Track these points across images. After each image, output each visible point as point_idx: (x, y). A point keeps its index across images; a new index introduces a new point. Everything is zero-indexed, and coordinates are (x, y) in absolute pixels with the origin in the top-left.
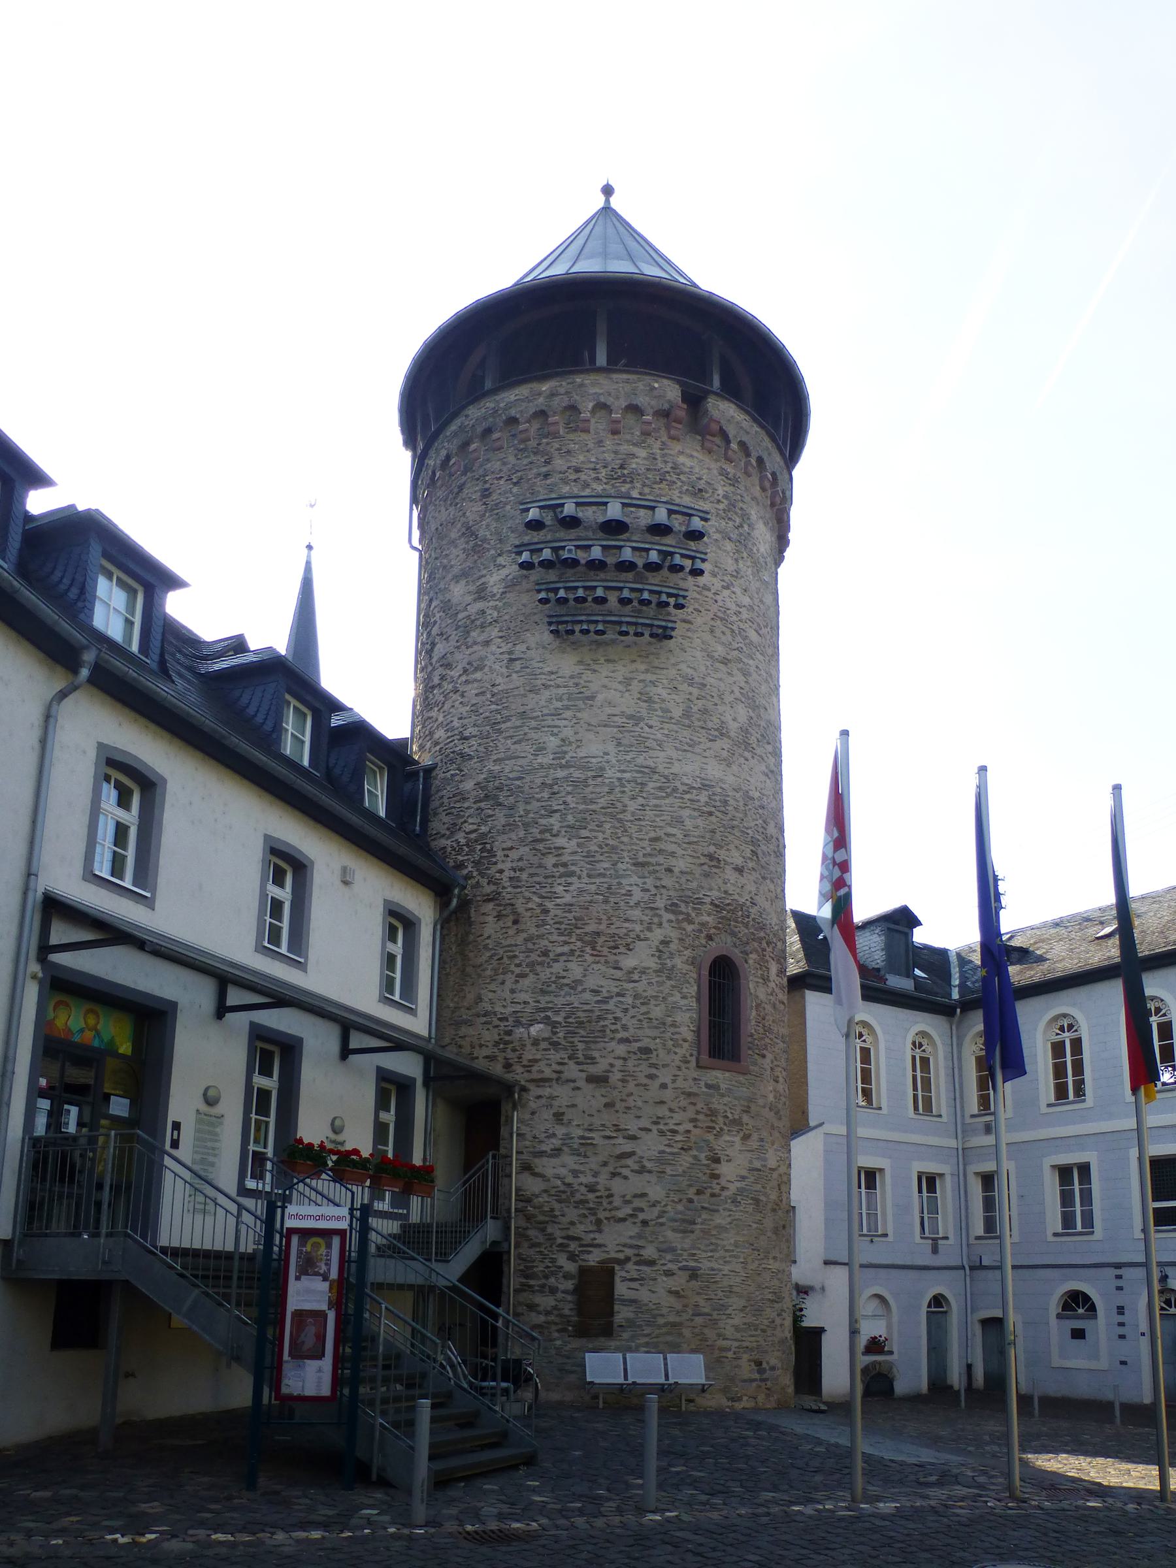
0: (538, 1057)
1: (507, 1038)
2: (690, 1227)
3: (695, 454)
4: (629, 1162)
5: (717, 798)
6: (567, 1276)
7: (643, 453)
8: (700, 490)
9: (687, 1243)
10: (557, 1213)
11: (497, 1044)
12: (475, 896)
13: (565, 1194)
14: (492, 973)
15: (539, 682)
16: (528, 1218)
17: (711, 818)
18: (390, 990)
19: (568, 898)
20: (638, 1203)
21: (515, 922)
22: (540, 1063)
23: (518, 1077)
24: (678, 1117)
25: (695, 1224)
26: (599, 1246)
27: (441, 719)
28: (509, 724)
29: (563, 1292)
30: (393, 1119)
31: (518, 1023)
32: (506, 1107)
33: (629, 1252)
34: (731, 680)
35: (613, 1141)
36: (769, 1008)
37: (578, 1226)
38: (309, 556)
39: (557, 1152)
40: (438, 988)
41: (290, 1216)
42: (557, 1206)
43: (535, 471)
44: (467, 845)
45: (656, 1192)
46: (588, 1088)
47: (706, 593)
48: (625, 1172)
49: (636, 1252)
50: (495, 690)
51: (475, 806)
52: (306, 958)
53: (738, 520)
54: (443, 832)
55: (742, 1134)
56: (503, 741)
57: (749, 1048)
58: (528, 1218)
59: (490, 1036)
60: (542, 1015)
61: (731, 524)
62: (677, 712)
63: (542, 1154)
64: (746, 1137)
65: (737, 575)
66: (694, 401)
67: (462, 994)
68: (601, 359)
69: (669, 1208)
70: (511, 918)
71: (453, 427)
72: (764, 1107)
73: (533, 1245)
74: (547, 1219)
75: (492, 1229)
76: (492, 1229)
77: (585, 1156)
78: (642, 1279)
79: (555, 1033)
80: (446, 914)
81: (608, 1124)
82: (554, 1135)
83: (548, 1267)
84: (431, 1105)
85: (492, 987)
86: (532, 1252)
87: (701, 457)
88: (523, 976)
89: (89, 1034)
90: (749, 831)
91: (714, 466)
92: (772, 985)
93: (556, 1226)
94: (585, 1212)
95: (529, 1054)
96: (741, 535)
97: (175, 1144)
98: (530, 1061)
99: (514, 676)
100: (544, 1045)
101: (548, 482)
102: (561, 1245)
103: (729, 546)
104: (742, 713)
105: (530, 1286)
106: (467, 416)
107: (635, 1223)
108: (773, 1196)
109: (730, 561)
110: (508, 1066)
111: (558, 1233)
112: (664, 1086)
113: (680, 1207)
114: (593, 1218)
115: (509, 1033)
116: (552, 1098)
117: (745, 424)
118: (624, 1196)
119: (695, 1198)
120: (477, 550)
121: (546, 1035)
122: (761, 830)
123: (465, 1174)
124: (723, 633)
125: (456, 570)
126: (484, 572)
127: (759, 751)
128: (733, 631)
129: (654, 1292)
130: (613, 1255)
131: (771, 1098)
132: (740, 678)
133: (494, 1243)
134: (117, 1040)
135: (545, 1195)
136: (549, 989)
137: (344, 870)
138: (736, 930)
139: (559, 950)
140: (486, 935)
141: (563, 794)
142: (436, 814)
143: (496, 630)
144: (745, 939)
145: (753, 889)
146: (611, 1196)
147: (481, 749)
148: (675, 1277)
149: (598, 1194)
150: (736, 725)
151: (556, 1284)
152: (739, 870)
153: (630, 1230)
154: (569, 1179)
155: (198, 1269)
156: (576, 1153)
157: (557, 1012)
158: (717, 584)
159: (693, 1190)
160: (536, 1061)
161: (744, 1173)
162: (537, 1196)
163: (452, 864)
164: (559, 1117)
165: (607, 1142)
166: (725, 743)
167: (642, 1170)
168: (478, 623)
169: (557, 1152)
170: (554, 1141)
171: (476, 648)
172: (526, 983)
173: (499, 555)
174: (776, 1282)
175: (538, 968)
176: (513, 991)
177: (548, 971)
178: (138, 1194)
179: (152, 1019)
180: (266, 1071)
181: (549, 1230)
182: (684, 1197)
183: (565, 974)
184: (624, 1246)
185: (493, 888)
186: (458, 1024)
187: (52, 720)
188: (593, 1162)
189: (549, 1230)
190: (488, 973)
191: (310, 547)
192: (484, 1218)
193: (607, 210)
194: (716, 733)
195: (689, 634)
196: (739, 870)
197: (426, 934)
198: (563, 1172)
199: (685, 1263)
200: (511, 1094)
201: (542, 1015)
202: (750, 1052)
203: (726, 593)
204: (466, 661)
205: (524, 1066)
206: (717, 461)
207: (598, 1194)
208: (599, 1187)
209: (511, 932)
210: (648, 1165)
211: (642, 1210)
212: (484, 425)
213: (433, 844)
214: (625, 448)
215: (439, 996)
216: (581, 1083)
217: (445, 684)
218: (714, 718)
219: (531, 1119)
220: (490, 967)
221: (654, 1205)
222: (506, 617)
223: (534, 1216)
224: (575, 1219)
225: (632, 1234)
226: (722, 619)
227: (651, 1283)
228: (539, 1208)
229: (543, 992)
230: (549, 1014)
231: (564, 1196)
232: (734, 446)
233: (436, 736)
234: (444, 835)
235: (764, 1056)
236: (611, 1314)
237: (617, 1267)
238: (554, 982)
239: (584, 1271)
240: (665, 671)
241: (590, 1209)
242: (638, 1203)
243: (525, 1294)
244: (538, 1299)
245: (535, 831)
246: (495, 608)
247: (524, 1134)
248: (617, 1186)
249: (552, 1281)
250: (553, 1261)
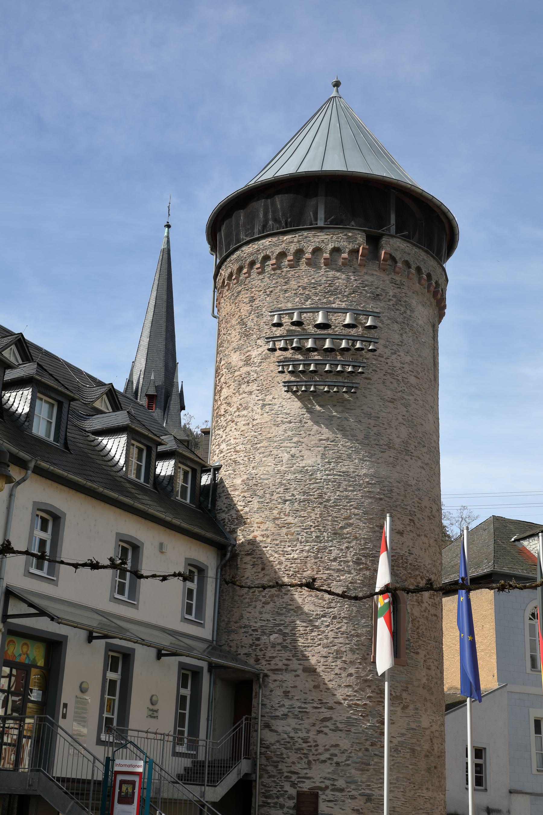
0: (274, 655)
1: (257, 642)
2: (366, 767)
3: (375, 273)
4: (328, 724)
5: (386, 489)
6: (290, 798)
8: (378, 295)
9: (365, 778)
10: (285, 756)
11: (251, 646)
12: (240, 551)
13: (289, 744)
14: (249, 601)
15: (279, 419)
16: (268, 758)
17: (381, 502)
18: (189, 612)
20: (333, 751)
21: (263, 569)
22: (276, 659)
23: (263, 668)
25: (369, 765)
26: (309, 778)
27: (224, 437)
28: (262, 445)
29: (287, 808)
30: (189, 693)
31: (264, 633)
32: (255, 687)
33: (328, 783)
34: (396, 411)
35: (318, 710)
36: (422, 621)
37: (297, 764)
39: (285, 716)
40: (219, 609)
41: (117, 765)
42: (284, 751)
43: (279, 288)
44: (237, 519)
45: (345, 744)
46: (303, 675)
47: (380, 359)
48: (326, 730)
49: (332, 782)
50: (255, 423)
51: (242, 495)
52: (138, 603)
53: (403, 309)
54: (224, 509)
55: (402, 705)
56: (258, 455)
57: (407, 649)
58: (268, 758)
59: (248, 641)
60: (278, 628)
61: (398, 312)
63: (276, 717)
64: (405, 708)
65: (401, 344)
66: (374, 241)
67: (232, 613)
69: (353, 754)
70: (261, 566)
71: (234, 256)
72: (418, 687)
73: (270, 777)
74: (279, 759)
75: (244, 766)
76: (244, 766)
77: (302, 719)
78: (336, 801)
79: (285, 640)
80: (224, 562)
81: (316, 699)
82: (284, 705)
83: (279, 791)
85: (249, 609)
86: (269, 781)
87: (378, 274)
89: (24, 657)
90: (408, 507)
91: (387, 278)
92: (425, 605)
93: (284, 764)
94: (302, 756)
95: (270, 653)
96: (405, 317)
97: (64, 716)
98: (270, 657)
99: (265, 415)
100: (279, 647)
101: (287, 295)
102: (287, 777)
103: (396, 327)
104: (404, 431)
105: (269, 803)
106: (242, 251)
107: (331, 764)
108: (426, 747)
109: (397, 336)
110: (257, 660)
111: (285, 769)
113: (360, 754)
114: (306, 760)
115: (258, 639)
116: (283, 681)
117: (407, 250)
118: (325, 746)
119: (370, 748)
120: (246, 335)
121: (280, 641)
122: (416, 505)
123: (234, 726)
124: (391, 383)
125: (234, 345)
126: (250, 348)
127: (415, 454)
128: (398, 380)
129: (343, 810)
130: (318, 784)
131: (424, 680)
132: (403, 409)
133: (246, 775)
134: (37, 658)
135: (278, 744)
136: (282, 612)
137: (161, 545)
138: (398, 572)
140: (246, 576)
141: (292, 490)
142: (220, 497)
143: (256, 385)
144: (404, 577)
145: (411, 544)
146: (317, 745)
147: (246, 459)
148: (357, 800)
149: (309, 744)
150: (400, 440)
151: (283, 802)
153: (328, 768)
154: (292, 734)
155: (74, 790)
156: (296, 717)
157: (286, 627)
158: (388, 352)
159: (368, 743)
160: (274, 657)
161: (404, 731)
162: (273, 745)
163: (228, 530)
164: (286, 694)
165: (315, 710)
166: (392, 453)
167: (336, 730)
168: (246, 380)
169: (285, 716)
170: (283, 709)
171: (244, 395)
172: (268, 607)
173: (258, 339)
174: (428, 805)
175: (276, 599)
176: (261, 613)
177: (281, 600)
179: (54, 647)
180: (114, 669)
181: (280, 767)
182: (362, 747)
183: (291, 603)
184: (325, 779)
185: (251, 547)
186: (229, 632)
187: (13, 497)
188: (307, 723)
189: (280, 767)
190: (247, 600)
191: (168, 226)
192: (239, 758)
194: (386, 447)
195: (369, 386)
197: (211, 573)
198: (288, 729)
199: (363, 791)
200: (258, 679)
201: (278, 628)
202: (408, 651)
203: (394, 357)
204: (238, 403)
205: (266, 661)
206: (388, 275)
207: (309, 744)
208: (310, 740)
209: (261, 575)
210: (339, 725)
211: (336, 755)
212: (251, 258)
213: (218, 515)
215: (219, 613)
216: (299, 672)
217: (227, 415)
218: (384, 438)
219: (271, 695)
220: (248, 597)
221: (343, 753)
222: (262, 378)
223: (272, 758)
224: (295, 760)
225: (330, 771)
226: (390, 374)
227: (341, 803)
228: (274, 752)
229: (279, 614)
230: (281, 628)
231: (289, 745)
232: (399, 264)
233: (222, 447)
234: (224, 511)
235: (417, 653)
237: (320, 793)
238: (284, 608)
239: (300, 794)
240: (353, 411)
241: (304, 754)
242: (333, 751)
243: (265, 808)
245: (275, 512)
246: (256, 372)
247: (265, 705)
248: (321, 739)
250: (282, 787)
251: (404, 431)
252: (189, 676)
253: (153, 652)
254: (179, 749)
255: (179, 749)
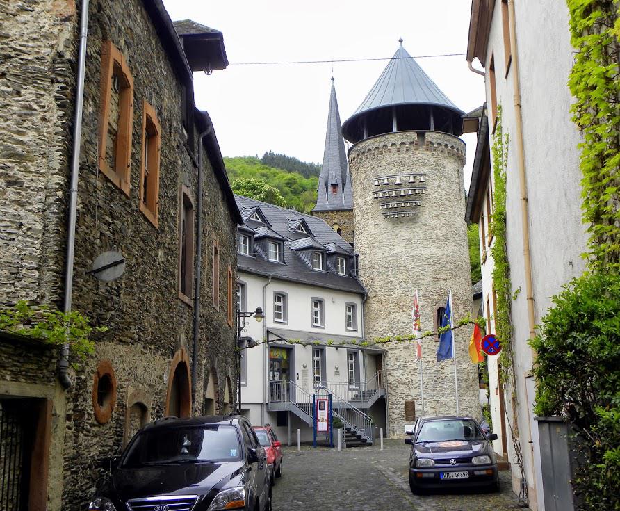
7: (407, 156)
9: (435, 393)
13: (400, 381)
19: (395, 296)
24: (429, 357)
38: (333, 88)
48: (416, 374)
62: (422, 236)
66: (421, 135)
68: (395, 130)
76: (379, 393)
84: (365, 357)
88: (384, 319)
97: (298, 378)
103: (436, 178)
112: (425, 348)
120: (364, 189)
139: (393, 311)
152: (445, 280)
153: (418, 391)
172: (385, 321)
178: (291, 391)
179: (289, 350)
180: (317, 356)
191: (333, 79)
193: (401, 50)
196: (445, 280)
203: (436, 193)
214: (402, 155)
236: (415, 414)
244: (395, 411)
249: (398, 406)
251: (444, 229)
252: (352, 354)
253: (335, 348)
254: (351, 387)
255: (351, 387)
